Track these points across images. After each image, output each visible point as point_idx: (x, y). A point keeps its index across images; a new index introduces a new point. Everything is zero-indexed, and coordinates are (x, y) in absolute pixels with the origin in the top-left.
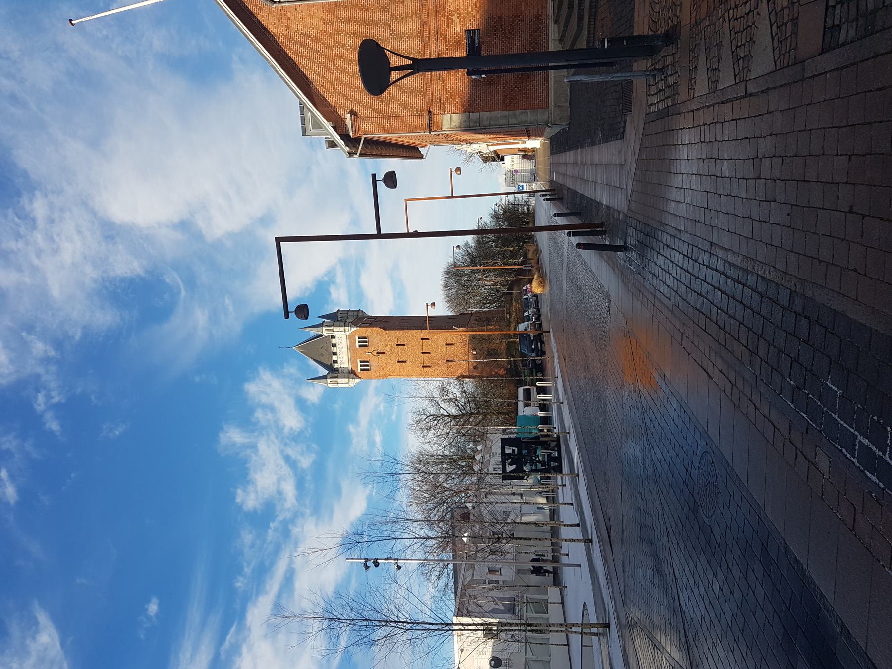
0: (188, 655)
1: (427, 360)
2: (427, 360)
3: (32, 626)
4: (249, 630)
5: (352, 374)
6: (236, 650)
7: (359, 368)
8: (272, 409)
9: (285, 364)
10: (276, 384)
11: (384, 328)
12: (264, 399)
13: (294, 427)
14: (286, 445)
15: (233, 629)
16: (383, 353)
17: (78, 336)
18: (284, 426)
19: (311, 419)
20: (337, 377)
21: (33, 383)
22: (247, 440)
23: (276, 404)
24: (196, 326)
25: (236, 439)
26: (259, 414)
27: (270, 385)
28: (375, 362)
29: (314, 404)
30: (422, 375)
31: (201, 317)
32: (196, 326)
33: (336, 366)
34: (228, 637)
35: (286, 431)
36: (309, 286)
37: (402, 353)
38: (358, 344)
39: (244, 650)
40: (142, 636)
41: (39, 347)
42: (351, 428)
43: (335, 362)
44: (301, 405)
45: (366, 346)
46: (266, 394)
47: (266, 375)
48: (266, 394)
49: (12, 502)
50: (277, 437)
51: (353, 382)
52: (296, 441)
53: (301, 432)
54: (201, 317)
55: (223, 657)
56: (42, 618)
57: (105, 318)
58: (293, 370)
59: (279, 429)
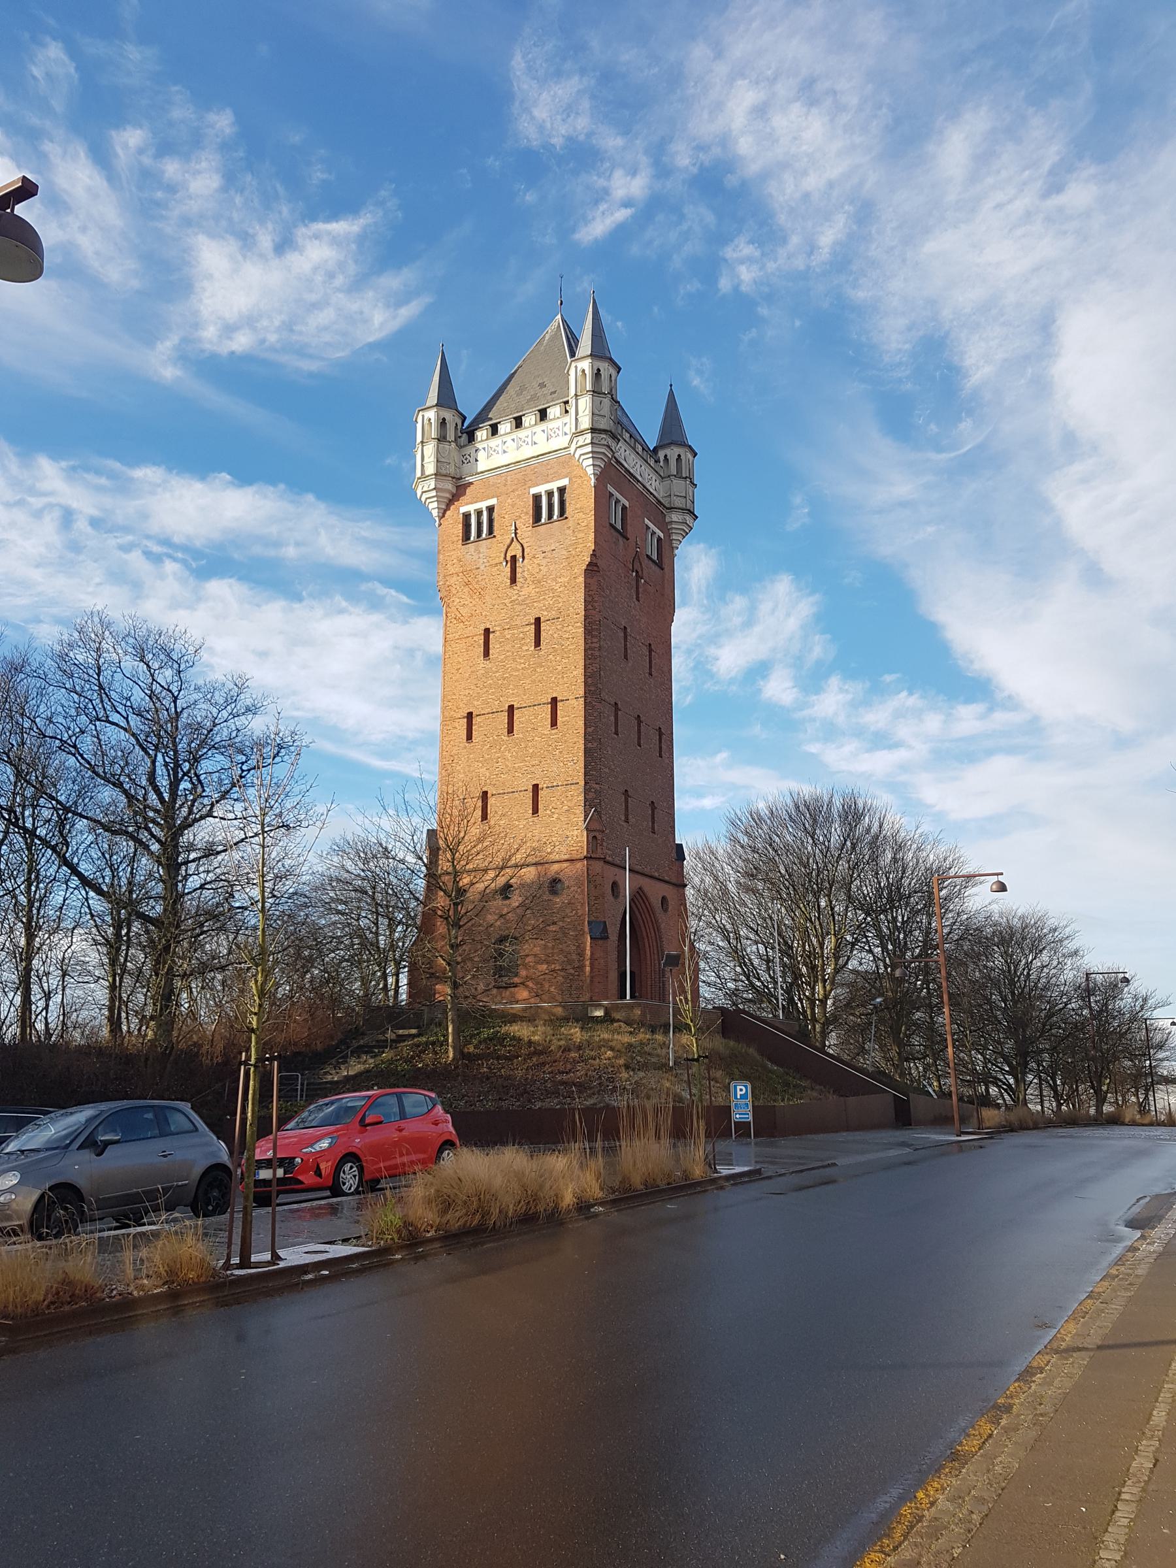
0: (364, 533)
1: (490, 727)
2: (490, 727)
3: (398, 300)
4: (406, 622)
5: (456, 487)
6: (375, 604)
7: (471, 508)
8: (749, 622)
9: (828, 636)
10: (792, 624)
11: (592, 569)
12: (765, 607)
13: (719, 662)
14: (689, 652)
15: (405, 599)
16: (513, 580)
17: (861, 295)
18: (720, 647)
19: (734, 688)
20: (442, 439)
21: (769, 236)
22: (694, 589)
23: (757, 629)
24: (884, 488)
25: (695, 570)
26: (739, 602)
27: (788, 615)
28: (487, 555)
29: (760, 690)
30: (446, 721)
31: (903, 488)
32: (884, 488)
33: (481, 434)
34: (393, 592)
35: (712, 651)
36: (976, 666)
37: (513, 643)
38: (541, 489)
39: (376, 617)
40: (388, 461)
41: (828, 237)
42: (723, 756)
43: (494, 430)
44: (759, 670)
45: (537, 517)
46: (773, 611)
47: (806, 608)
48: (773, 611)
49: (577, 236)
50: (700, 637)
51: (426, 491)
52: (695, 668)
53: (711, 675)
54: (903, 488)
55: (364, 587)
56: (407, 312)
57: (893, 337)
58: (817, 652)
59: (714, 639)
